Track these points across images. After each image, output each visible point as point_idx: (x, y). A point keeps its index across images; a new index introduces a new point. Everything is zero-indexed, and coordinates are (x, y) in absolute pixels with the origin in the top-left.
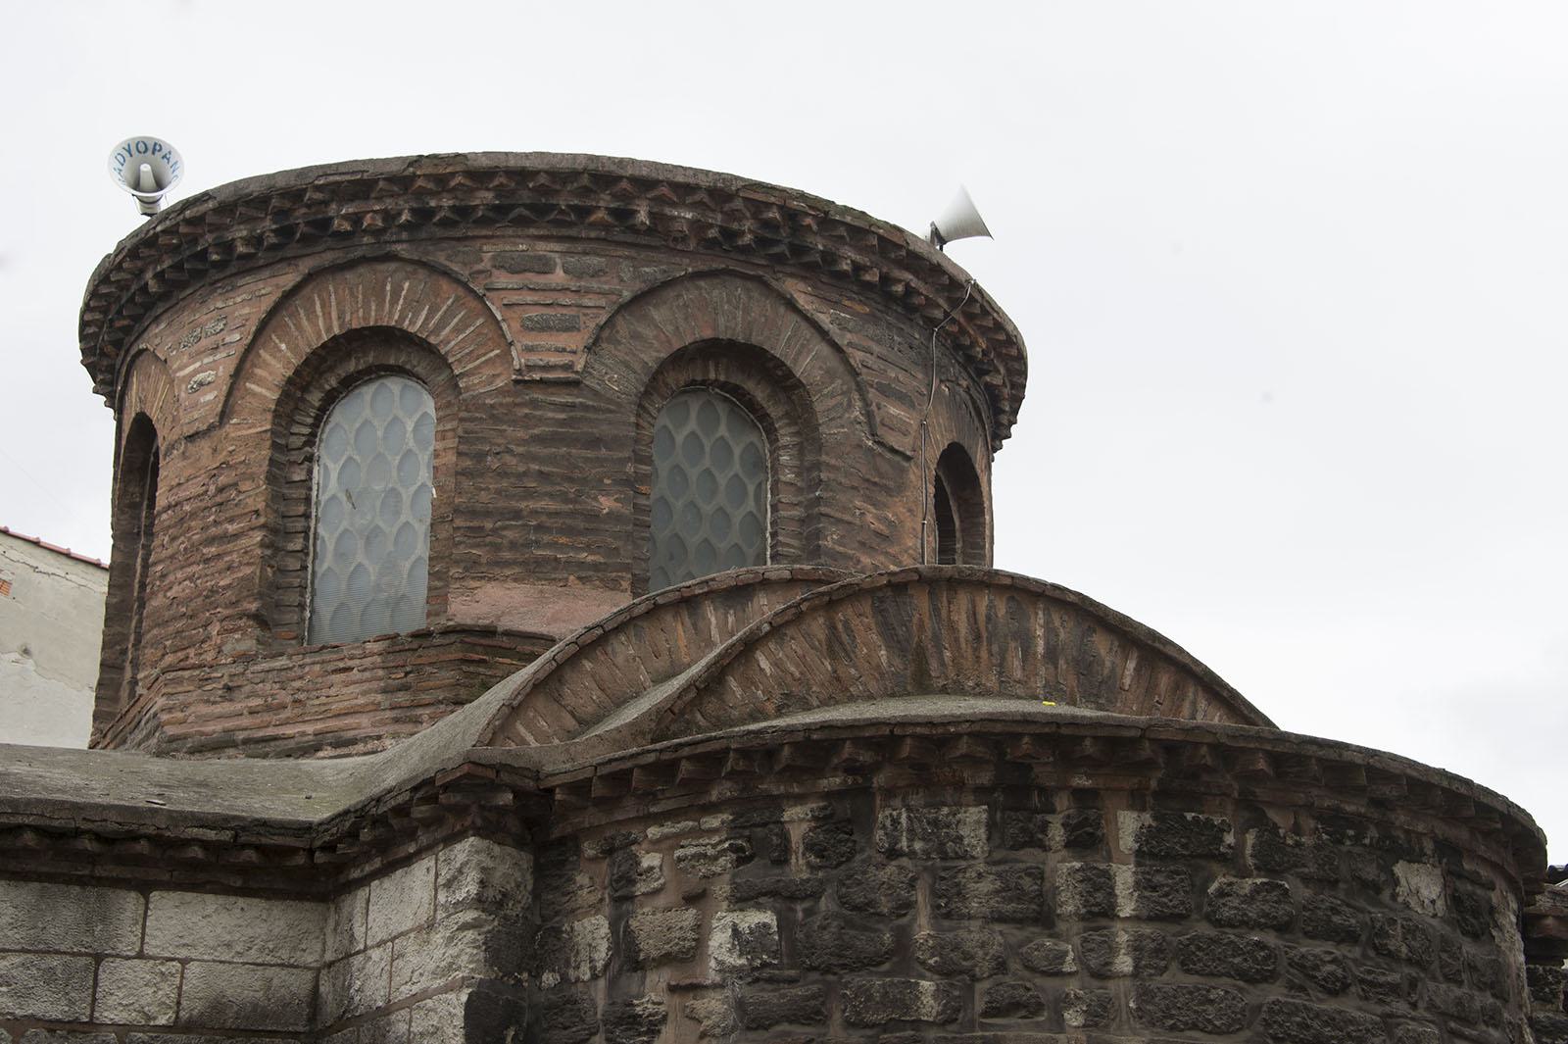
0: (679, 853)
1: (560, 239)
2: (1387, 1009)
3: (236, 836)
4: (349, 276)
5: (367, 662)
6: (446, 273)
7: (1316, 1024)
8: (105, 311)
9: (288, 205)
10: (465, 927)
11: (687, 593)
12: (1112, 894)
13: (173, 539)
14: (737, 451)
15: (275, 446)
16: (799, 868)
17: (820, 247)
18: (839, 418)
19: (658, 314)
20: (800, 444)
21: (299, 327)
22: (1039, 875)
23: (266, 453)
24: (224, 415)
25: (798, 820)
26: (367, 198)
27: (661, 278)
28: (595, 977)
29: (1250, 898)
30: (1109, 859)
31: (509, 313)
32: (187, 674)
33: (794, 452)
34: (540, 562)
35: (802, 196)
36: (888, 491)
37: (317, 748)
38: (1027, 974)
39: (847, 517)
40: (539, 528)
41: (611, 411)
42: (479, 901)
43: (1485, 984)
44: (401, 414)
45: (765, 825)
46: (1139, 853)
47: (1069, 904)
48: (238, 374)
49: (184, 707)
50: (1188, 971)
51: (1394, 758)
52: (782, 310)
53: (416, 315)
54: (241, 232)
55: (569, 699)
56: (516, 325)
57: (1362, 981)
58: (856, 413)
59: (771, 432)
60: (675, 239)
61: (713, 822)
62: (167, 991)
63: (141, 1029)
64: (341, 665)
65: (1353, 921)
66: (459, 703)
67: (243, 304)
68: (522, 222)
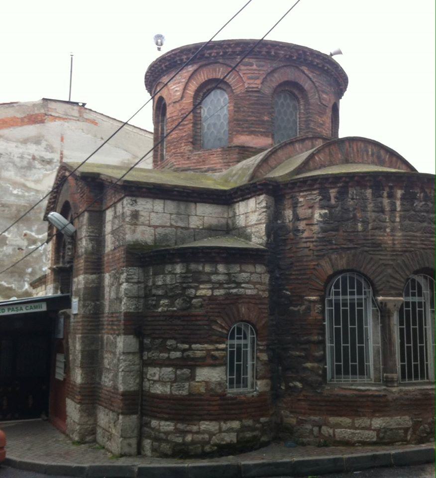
0: (307, 198)
4: (209, 67)
5: (218, 153)
8: (151, 73)
12: (396, 206)
13: (172, 125)
16: (333, 201)
17: (310, 59)
18: (313, 99)
19: (276, 75)
21: (198, 79)
22: (381, 203)
24: (182, 98)
25: (333, 192)
27: (277, 67)
28: (290, 222)
29: (421, 207)
30: (395, 199)
35: (307, 48)
36: (322, 114)
37: (209, 171)
38: (379, 222)
39: (315, 120)
42: (266, 207)
47: (387, 208)
48: (185, 89)
49: (179, 161)
50: (410, 221)
52: (301, 74)
55: (270, 163)
58: (317, 97)
61: (315, 192)
62: (201, 222)
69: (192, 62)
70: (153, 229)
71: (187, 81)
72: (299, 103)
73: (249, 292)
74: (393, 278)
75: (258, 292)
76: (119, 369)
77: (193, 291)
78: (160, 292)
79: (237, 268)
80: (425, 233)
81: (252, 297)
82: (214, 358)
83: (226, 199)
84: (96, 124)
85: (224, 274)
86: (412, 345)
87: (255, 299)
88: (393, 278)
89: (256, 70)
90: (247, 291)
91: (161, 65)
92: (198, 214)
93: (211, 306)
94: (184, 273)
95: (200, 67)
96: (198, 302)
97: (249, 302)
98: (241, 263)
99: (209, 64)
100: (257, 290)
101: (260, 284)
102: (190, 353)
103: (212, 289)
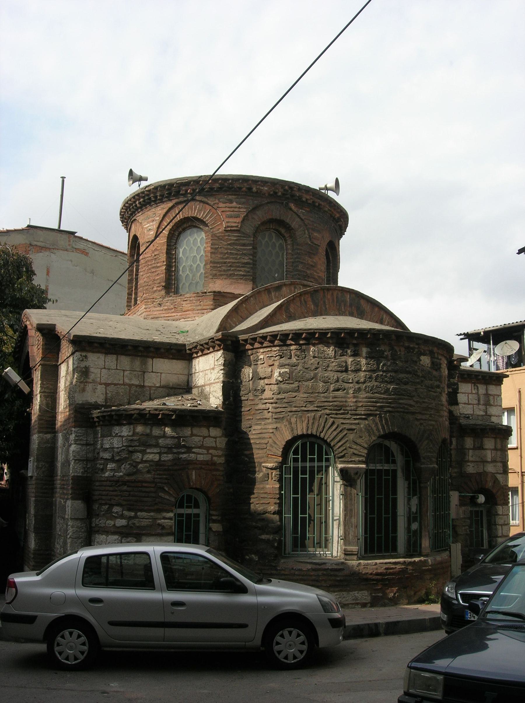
0: (267, 355)
1: (235, 195)
8: (126, 210)
10: (221, 370)
12: (361, 366)
14: (277, 246)
15: (167, 245)
23: (165, 247)
26: (189, 185)
29: (390, 366)
31: (223, 213)
34: (230, 275)
39: (304, 261)
40: (230, 266)
44: (197, 238)
51: (421, 334)
56: (224, 216)
59: (286, 240)
63: (153, 387)
66: (213, 309)
67: (160, 210)
69: (169, 198)
70: (104, 386)
71: (161, 219)
73: (201, 458)
74: (356, 443)
75: (212, 458)
76: (67, 536)
77: (140, 455)
78: (107, 455)
79: (187, 431)
81: (202, 463)
82: (163, 528)
84: (87, 254)
87: (208, 464)
88: (356, 443)
89: (236, 207)
91: (135, 202)
94: (130, 436)
96: (146, 467)
97: (201, 468)
98: (192, 426)
101: (215, 448)
102: (136, 521)
103: (160, 454)
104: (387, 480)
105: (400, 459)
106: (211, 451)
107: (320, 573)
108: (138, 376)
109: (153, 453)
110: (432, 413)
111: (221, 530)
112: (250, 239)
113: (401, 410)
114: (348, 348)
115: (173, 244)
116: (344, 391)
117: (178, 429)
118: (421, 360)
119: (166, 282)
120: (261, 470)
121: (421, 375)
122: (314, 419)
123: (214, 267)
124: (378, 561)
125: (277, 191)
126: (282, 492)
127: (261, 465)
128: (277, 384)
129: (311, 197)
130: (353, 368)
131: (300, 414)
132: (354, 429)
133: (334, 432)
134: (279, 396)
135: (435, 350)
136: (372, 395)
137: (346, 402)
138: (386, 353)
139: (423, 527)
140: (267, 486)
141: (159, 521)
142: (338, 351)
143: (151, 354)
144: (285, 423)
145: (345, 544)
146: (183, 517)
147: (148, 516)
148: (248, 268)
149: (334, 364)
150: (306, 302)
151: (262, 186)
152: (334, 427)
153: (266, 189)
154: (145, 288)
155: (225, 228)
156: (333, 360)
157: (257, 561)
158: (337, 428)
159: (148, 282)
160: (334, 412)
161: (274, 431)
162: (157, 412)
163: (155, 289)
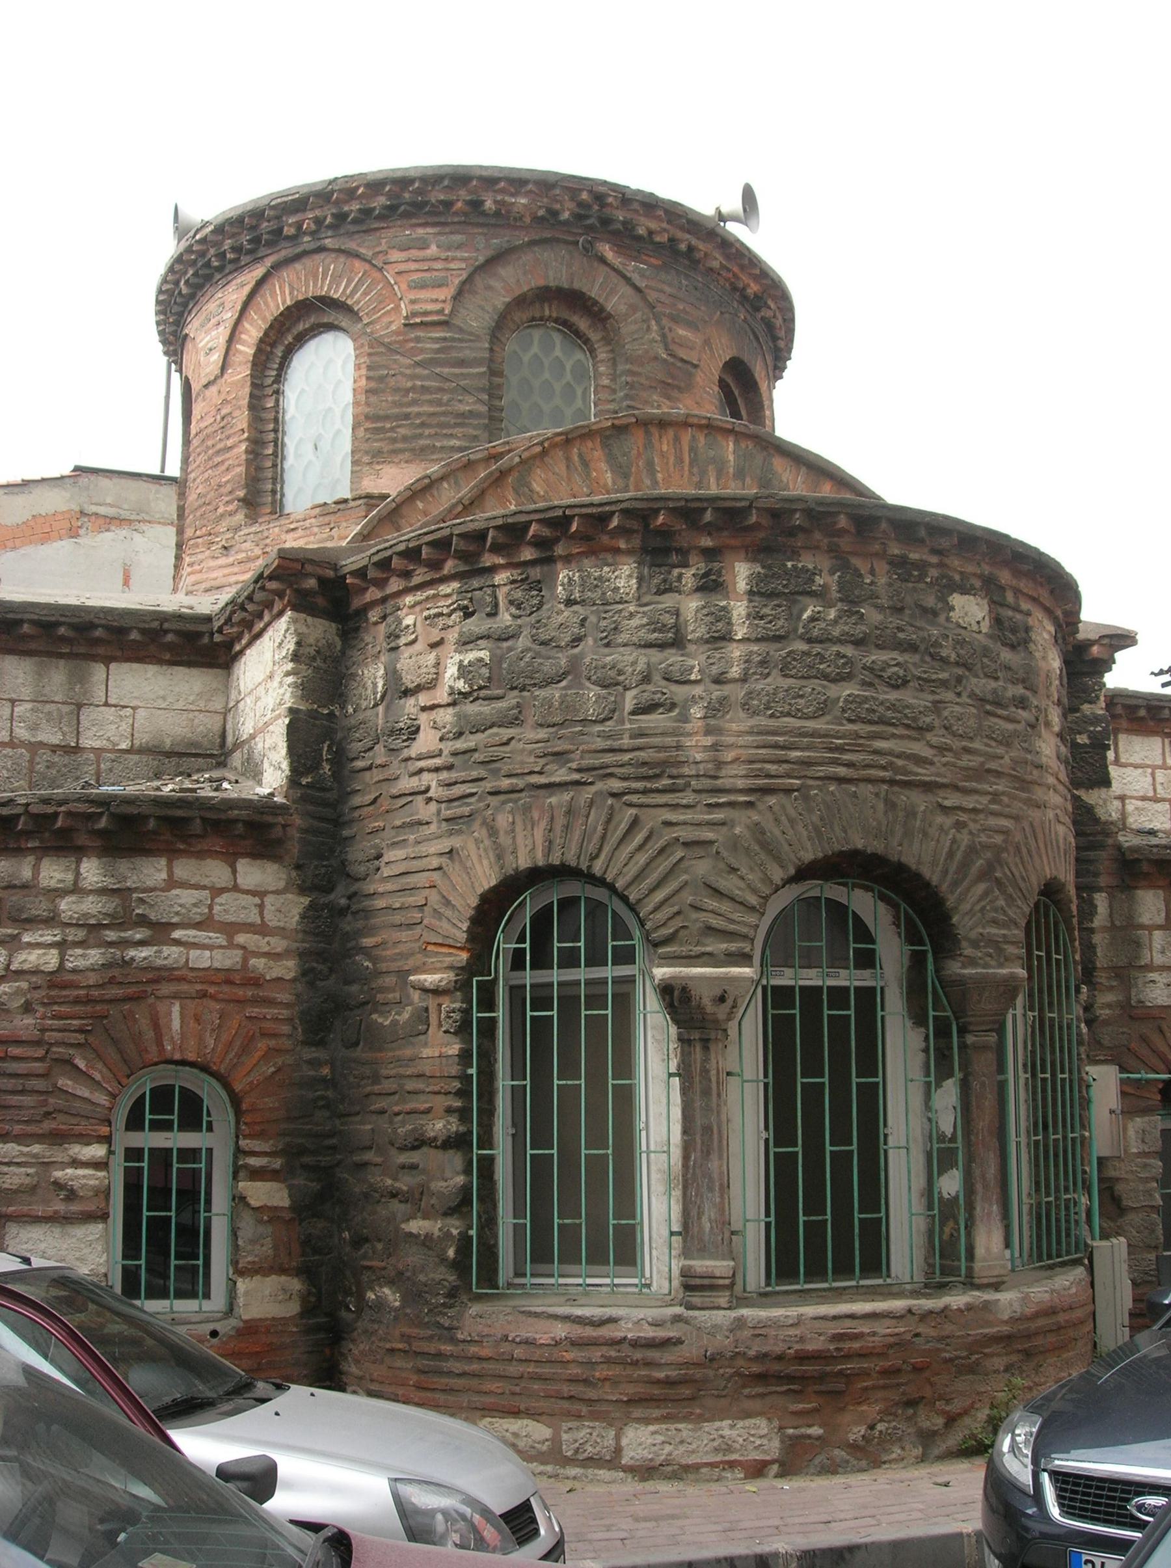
0: (426, 613)
2: (937, 697)
3: (161, 625)
6: (357, 256)
7: (881, 709)
9: (254, 222)
10: (288, 674)
11: (493, 451)
12: (730, 623)
14: (568, 367)
15: (253, 385)
20: (614, 359)
21: (266, 303)
23: (247, 390)
24: (223, 369)
26: (304, 210)
27: (505, 245)
29: (835, 622)
31: (399, 279)
32: (200, 540)
33: (609, 364)
34: (423, 449)
38: (664, 683)
40: (423, 425)
41: (471, 341)
43: (1017, 679)
45: (481, 589)
46: (751, 593)
48: (231, 339)
52: (596, 264)
53: (338, 287)
54: (228, 243)
56: (404, 286)
57: (919, 678)
58: (654, 335)
59: (592, 351)
60: (515, 219)
61: (445, 589)
62: (125, 727)
63: (109, 751)
64: (292, 526)
65: (914, 637)
67: (233, 294)
68: (406, 215)
72: (594, 357)
73: (201, 959)
74: (717, 893)
75: (245, 960)
79: (152, 872)
80: (850, 721)
81: (210, 976)
82: (72, 1195)
83: (203, 646)
85: (103, 891)
86: (529, 1152)
87: (229, 982)
88: (717, 893)
89: (436, 259)
90: (194, 954)
91: (177, 283)
92: (111, 701)
93: (56, 1008)
95: (276, 267)
96: (18, 992)
97: (204, 995)
98: (172, 853)
99: (297, 258)
100: (240, 952)
101: (262, 929)
103: (62, 946)
104: (840, 1025)
105: (891, 950)
106: (241, 939)
107: (596, 1354)
108: (61, 717)
109: (38, 945)
110: (1000, 788)
111: (286, 1203)
112: (478, 345)
113: (882, 774)
114: (686, 565)
115: (269, 381)
116: (670, 710)
117: (123, 866)
118: (952, 609)
119: (247, 486)
120: (408, 996)
121: (953, 656)
122: (569, 812)
123: (376, 431)
124: (810, 1310)
125: (558, 206)
126: (470, 1071)
127: (405, 982)
128: (453, 704)
129: (664, 225)
130: (701, 632)
131: (524, 798)
132: (711, 842)
133: (637, 857)
134: (460, 745)
135: (1005, 577)
136: (772, 723)
137: (678, 747)
138: (819, 580)
139: (979, 1187)
140: (426, 1052)
141: (58, 1174)
142: (651, 577)
143: (101, 651)
144: (480, 832)
145: (686, 1253)
146: (141, 1160)
147: (22, 1154)
148: (475, 427)
149: (635, 622)
150: (585, 464)
151: (512, 195)
152: (639, 838)
153: (523, 201)
154: (198, 514)
155: (406, 318)
156: (632, 608)
157: (396, 1310)
158: (647, 839)
159: (205, 496)
160: (639, 785)
161: (444, 861)
162: (50, 810)
163: (220, 511)
